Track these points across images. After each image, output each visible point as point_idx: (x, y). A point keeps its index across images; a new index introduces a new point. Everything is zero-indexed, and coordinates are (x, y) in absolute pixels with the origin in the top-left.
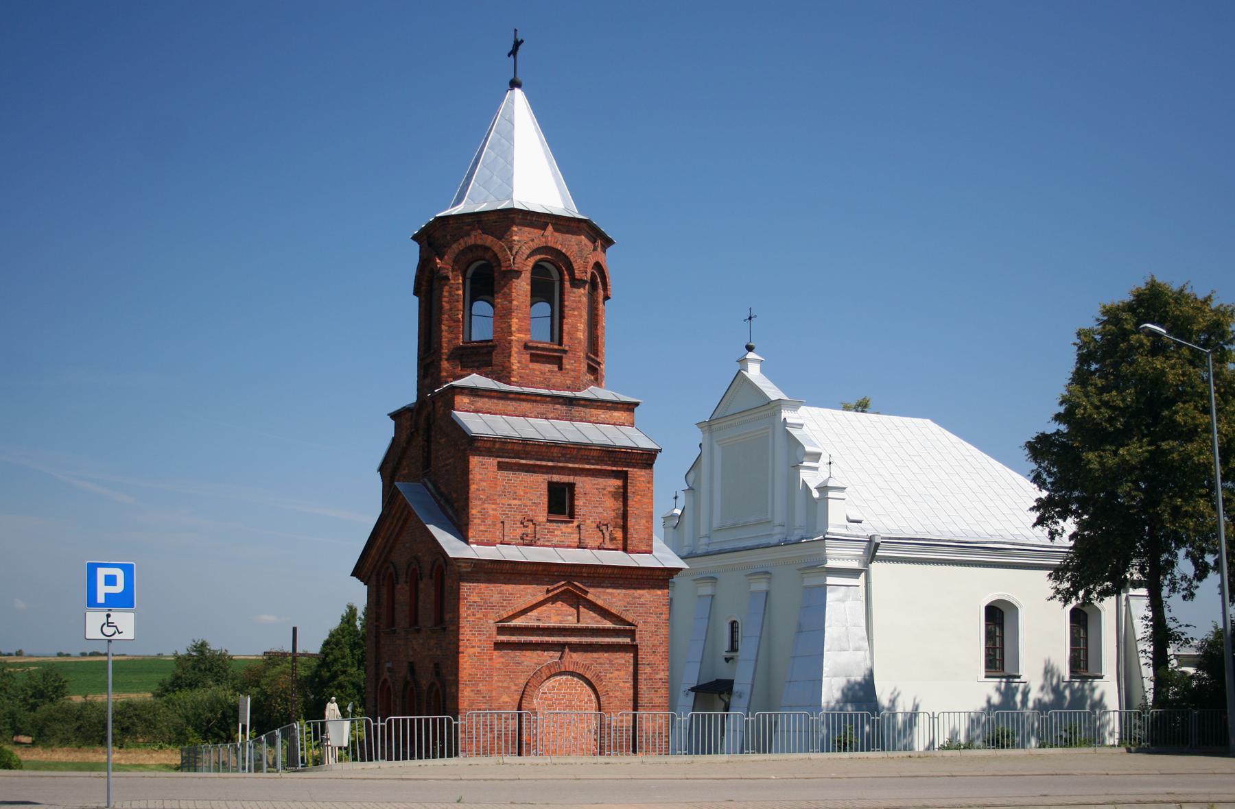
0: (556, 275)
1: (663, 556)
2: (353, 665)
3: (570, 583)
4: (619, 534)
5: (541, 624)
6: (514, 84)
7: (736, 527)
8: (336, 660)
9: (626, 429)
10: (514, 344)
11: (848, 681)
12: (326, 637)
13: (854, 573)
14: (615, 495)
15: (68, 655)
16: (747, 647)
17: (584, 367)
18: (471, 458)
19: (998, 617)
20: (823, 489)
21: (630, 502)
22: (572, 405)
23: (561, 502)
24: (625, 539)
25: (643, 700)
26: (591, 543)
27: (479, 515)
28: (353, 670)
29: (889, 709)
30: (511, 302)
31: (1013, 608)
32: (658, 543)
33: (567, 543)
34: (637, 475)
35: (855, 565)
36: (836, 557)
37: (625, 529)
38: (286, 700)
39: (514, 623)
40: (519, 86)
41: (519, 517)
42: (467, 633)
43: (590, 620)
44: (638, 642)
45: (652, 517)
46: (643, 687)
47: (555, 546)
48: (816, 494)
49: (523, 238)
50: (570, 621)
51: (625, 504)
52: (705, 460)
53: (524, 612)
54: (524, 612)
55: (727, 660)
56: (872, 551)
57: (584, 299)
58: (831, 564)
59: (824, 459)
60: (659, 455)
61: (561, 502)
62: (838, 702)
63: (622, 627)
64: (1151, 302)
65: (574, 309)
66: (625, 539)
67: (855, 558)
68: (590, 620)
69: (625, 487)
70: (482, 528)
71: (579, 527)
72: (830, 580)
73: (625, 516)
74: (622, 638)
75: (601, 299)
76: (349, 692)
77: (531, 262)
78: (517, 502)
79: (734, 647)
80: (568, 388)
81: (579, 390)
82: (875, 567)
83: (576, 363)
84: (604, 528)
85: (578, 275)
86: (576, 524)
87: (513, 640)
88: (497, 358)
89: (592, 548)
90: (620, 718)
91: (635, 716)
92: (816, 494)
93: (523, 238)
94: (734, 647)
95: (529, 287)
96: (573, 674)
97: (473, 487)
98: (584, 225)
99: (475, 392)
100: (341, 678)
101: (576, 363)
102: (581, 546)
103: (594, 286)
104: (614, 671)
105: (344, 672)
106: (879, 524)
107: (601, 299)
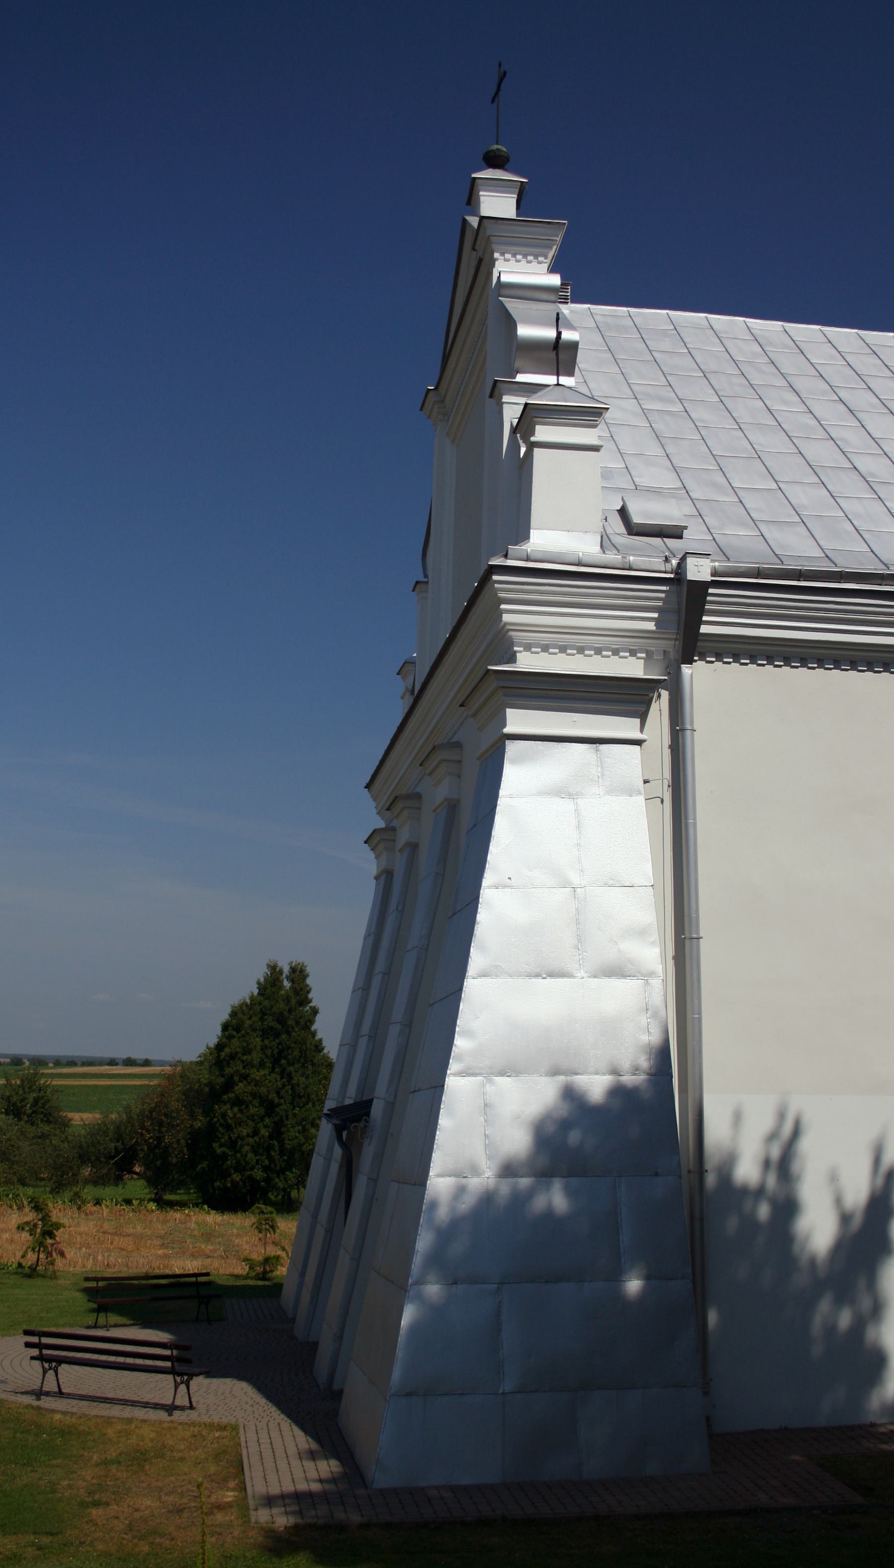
2: (262, 1065)
8: (232, 1057)
11: (570, 1094)
12: (225, 1016)
13: (626, 697)
15: (147, 1063)
28: (257, 1074)
29: (251, 1268)
35: (632, 668)
36: (545, 639)
38: (161, 1124)
56: (686, 617)
58: (528, 662)
62: (508, 1170)
67: (630, 642)
72: (518, 720)
76: (252, 1110)
82: (699, 676)
100: (240, 1087)
105: (244, 1077)
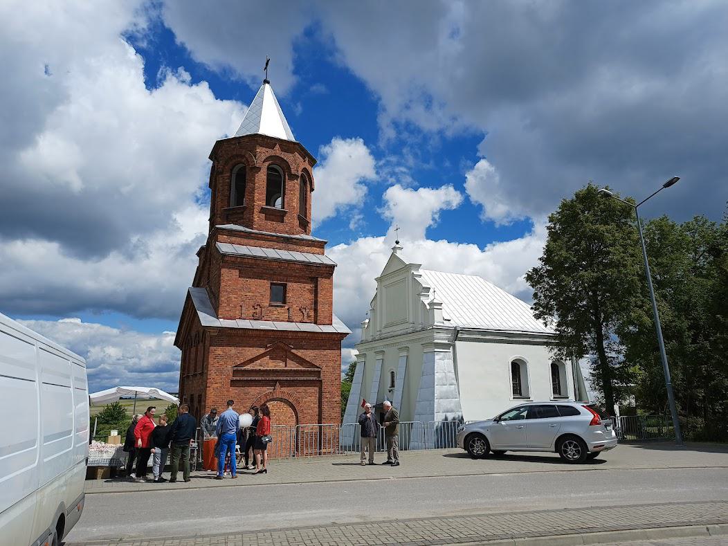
0: (282, 173)
1: (338, 326)
3: (279, 343)
4: (312, 313)
5: (262, 368)
6: (266, 82)
7: (392, 325)
9: (320, 256)
10: (256, 207)
14: (310, 291)
16: (399, 383)
17: (297, 222)
18: (223, 271)
19: (517, 368)
20: (431, 304)
21: (319, 295)
22: (288, 242)
23: (280, 296)
24: (316, 316)
25: (325, 414)
26: (296, 319)
27: (225, 301)
30: (254, 184)
31: (524, 363)
32: (335, 319)
33: (281, 319)
34: (322, 282)
37: (316, 310)
39: (249, 367)
40: (268, 83)
41: (252, 303)
42: (212, 373)
43: (292, 366)
44: (322, 378)
45: (332, 304)
46: (325, 407)
47: (273, 320)
48: (428, 307)
49: (262, 153)
50: (280, 365)
51: (316, 296)
52: (378, 295)
53: (252, 361)
54: (252, 361)
55: (390, 391)
57: (297, 186)
59: (431, 290)
60: (336, 268)
61: (280, 296)
63: (312, 369)
64: (588, 198)
65: (291, 191)
66: (316, 316)
68: (292, 366)
69: (316, 287)
70: (228, 309)
71: (288, 309)
73: (316, 303)
74: (311, 377)
75: (309, 189)
77: (267, 164)
78: (250, 294)
79: (393, 386)
80: (287, 233)
81: (293, 234)
83: (292, 220)
84: (304, 311)
85: (293, 172)
86: (286, 307)
87: (243, 378)
88: (246, 215)
89: (296, 322)
90: (310, 427)
91: (320, 427)
92: (428, 307)
93: (262, 153)
94: (393, 386)
95: (265, 177)
96: (281, 400)
97: (223, 284)
98: (297, 146)
99: (231, 233)
101: (292, 220)
102: (290, 320)
103: (304, 182)
104: (308, 397)
106: (458, 321)
107: (309, 189)
